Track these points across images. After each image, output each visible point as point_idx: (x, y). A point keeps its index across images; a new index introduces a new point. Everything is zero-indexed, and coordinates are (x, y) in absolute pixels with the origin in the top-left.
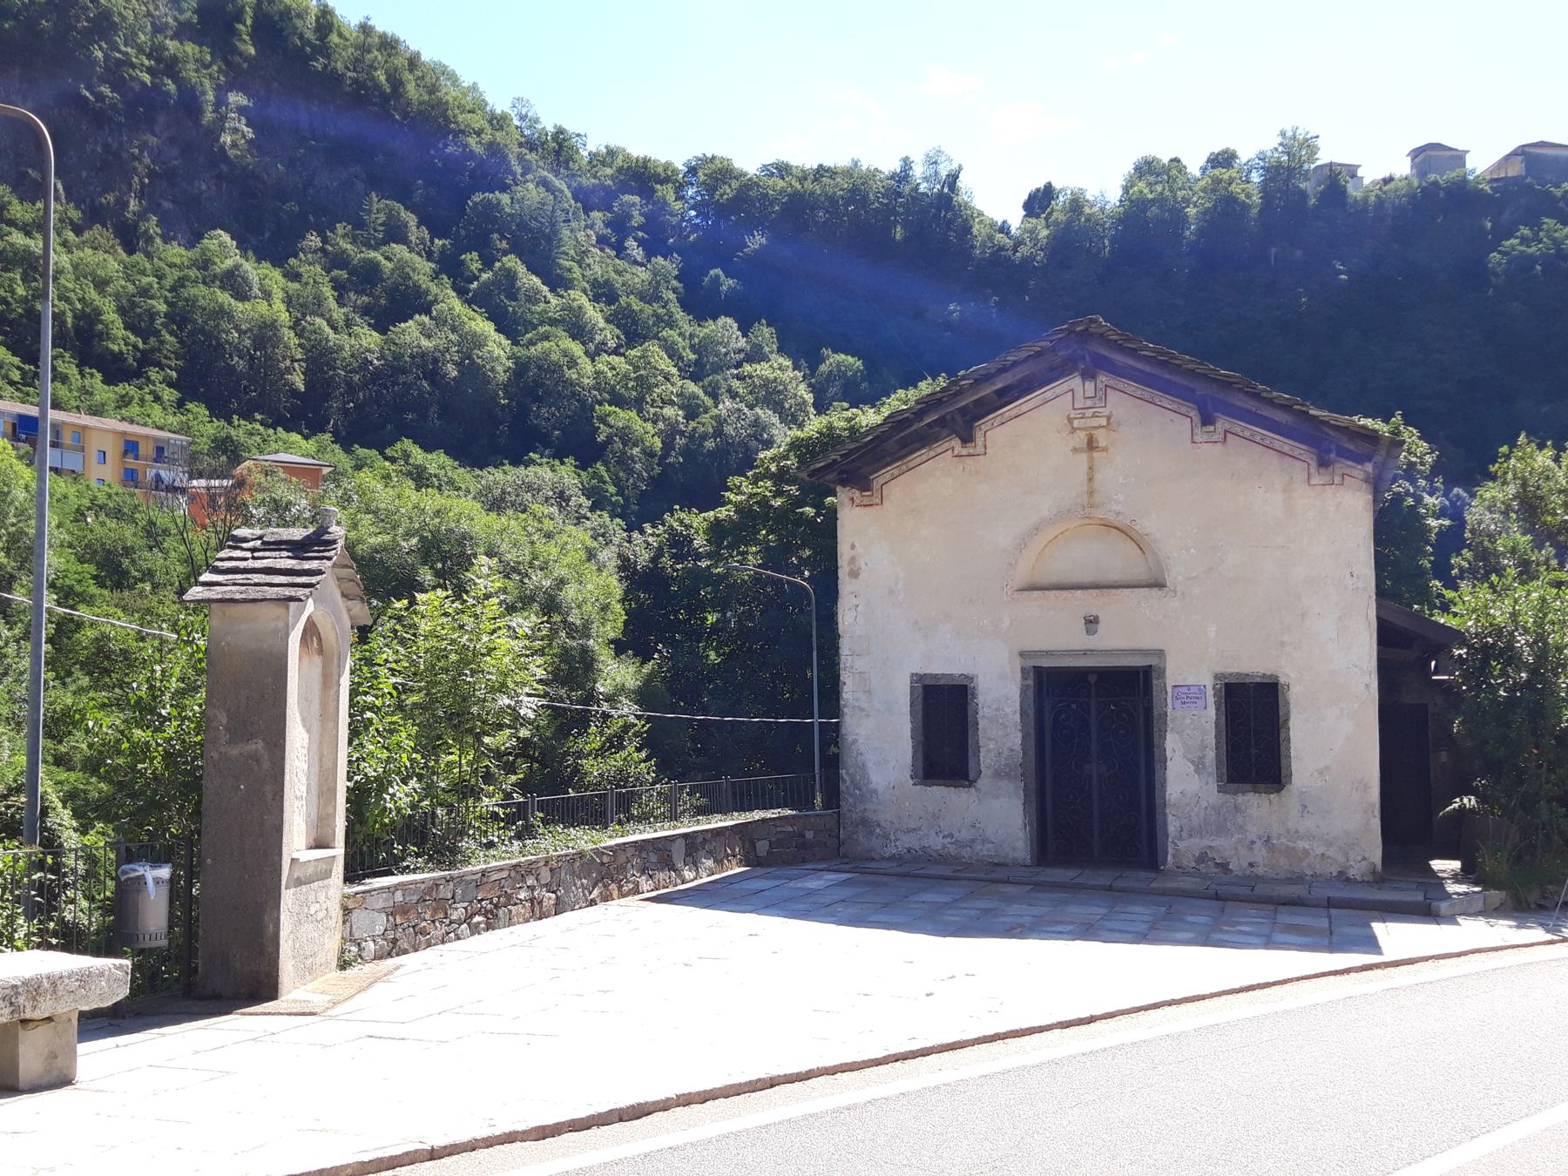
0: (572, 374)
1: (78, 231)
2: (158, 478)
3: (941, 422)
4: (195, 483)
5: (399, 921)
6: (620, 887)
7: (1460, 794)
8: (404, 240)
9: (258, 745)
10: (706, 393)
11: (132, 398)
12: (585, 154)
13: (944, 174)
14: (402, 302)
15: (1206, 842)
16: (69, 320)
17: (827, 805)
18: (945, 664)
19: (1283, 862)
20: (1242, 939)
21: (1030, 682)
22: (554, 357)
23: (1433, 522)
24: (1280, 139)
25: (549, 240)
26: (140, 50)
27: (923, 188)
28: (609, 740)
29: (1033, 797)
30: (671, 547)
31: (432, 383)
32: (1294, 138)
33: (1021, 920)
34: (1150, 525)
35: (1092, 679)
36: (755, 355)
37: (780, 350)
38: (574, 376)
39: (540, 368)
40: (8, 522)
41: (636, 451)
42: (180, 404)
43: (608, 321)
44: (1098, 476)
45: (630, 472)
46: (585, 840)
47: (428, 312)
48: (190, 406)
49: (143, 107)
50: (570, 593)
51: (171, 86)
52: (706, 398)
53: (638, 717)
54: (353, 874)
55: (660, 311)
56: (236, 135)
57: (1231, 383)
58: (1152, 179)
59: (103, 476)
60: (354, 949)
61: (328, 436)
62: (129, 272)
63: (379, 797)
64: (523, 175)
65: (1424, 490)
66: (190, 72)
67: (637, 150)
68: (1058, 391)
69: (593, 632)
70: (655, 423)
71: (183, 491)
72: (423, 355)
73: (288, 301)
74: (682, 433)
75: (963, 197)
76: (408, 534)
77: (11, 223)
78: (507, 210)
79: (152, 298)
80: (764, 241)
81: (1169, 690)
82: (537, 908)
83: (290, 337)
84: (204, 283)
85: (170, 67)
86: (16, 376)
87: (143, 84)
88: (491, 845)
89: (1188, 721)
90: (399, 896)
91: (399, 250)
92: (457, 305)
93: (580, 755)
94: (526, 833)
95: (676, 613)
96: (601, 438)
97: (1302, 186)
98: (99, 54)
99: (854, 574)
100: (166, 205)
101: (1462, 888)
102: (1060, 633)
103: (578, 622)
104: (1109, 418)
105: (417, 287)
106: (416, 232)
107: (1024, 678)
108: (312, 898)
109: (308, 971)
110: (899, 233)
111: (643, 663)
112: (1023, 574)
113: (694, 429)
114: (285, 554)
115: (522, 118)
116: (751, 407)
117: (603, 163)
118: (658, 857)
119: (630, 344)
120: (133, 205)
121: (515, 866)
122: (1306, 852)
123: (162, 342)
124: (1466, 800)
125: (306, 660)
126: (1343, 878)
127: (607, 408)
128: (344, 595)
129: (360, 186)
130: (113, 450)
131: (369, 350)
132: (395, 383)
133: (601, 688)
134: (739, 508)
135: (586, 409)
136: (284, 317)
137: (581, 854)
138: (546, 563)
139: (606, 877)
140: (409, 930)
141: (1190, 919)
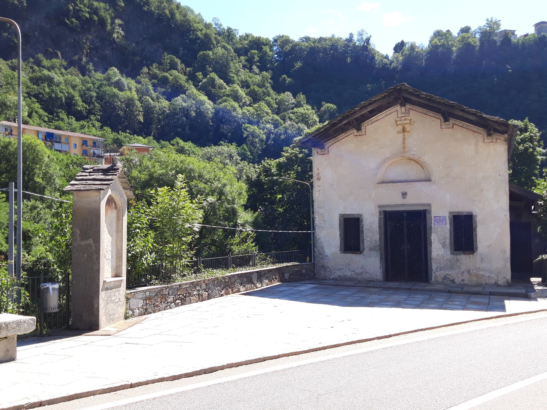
0: (235, 114)
1: (66, 69)
2: (94, 153)
3: (349, 123)
4: (106, 154)
5: (148, 302)
6: (232, 290)
7: (541, 254)
8: (176, 69)
9: (90, 241)
10: (281, 119)
11: (85, 126)
12: (238, 36)
13: (365, 38)
14: (177, 90)
15: (447, 272)
16: (64, 100)
17: (311, 261)
18: (351, 210)
19: (474, 279)
20: (454, 307)
21: (382, 216)
22: (228, 108)
23: (539, 157)
24: (486, 22)
25: (226, 67)
26: (85, 6)
27: (357, 44)
28: (242, 239)
29: (384, 257)
30: (264, 172)
31: (186, 118)
32: (491, 21)
33: (374, 301)
34: (426, 159)
35: (405, 215)
36: (298, 105)
37: (307, 103)
38: (235, 114)
39: (223, 112)
40: (42, 168)
41: (257, 140)
42: (101, 127)
43: (247, 94)
44: (407, 142)
45: (255, 147)
46: (219, 273)
47: (185, 93)
48: (105, 128)
49: (86, 24)
50: (228, 189)
51: (96, 18)
52: (281, 121)
53: (252, 231)
54: (129, 287)
55: (265, 90)
56: (118, 34)
57: (454, 106)
58: (440, 38)
59: (76, 152)
60: (131, 312)
61: (151, 137)
62: (84, 83)
63: (141, 259)
64: (217, 44)
65: (536, 146)
66: (102, 13)
67: (256, 34)
68: (392, 111)
69: (236, 202)
70: (263, 130)
71: (102, 157)
72: (183, 108)
73: (137, 91)
74: (273, 133)
75: (372, 46)
76: (171, 170)
77: (44, 67)
78: (211, 57)
79: (91, 91)
80: (301, 64)
81: (433, 218)
82: (201, 297)
83: (138, 103)
84: (109, 85)
85: (95, 11)
86: (46, 119)
87: (86, 17)
88: (184, 275)
89: (439, 229)
90: (148, 294)
91: (174, 72)
92: (195, 91)
93: (232, 245)
94: (197, 271)
95: (266, 195)
96: (245, 136)
97: (495, 38)
98: (71, 8)
99: (319, 179)
100: (96, 59)
101: (540, 288)
102: (393, 199)
103: (230, 199)
104: (410, 120)
105: (181, 85)
106: (180, 66)
107: (380, 215)
108: (113, 294)
109: (111, 320)
110: (349, 60)
111: (254, 213)
112: (380, 176)
113: (277, 132)
114: (101, 173)
115: (216, 24)
116: (297, 123)
117: (244, 39)
118: (247, 279)
119: (254, 103)
120: (84, 59)
121: (192, 283)
122: (483, 276)
123: (95, 106)
124: (544, 256)
125: (109, 211)
126: (497, 285)
127: (247, 125)
128: (123, 188)
129: (161, 50)
130: (79, 143)
131: (165, 107)
132: (174, 118)
133: (239, 221)
134: (287, 158)
135: (239, 126)
136: (136, 97)
137: (217, 279)
138: (219, 178)
139: (227, 286)
140: (151, 306)
141: (437, 300)
